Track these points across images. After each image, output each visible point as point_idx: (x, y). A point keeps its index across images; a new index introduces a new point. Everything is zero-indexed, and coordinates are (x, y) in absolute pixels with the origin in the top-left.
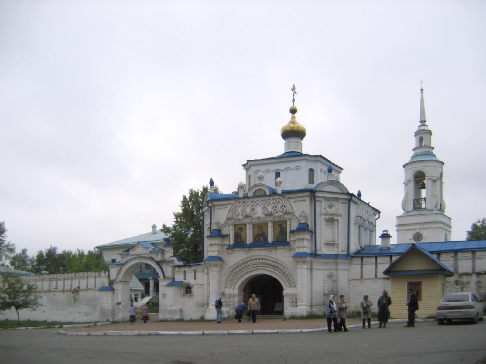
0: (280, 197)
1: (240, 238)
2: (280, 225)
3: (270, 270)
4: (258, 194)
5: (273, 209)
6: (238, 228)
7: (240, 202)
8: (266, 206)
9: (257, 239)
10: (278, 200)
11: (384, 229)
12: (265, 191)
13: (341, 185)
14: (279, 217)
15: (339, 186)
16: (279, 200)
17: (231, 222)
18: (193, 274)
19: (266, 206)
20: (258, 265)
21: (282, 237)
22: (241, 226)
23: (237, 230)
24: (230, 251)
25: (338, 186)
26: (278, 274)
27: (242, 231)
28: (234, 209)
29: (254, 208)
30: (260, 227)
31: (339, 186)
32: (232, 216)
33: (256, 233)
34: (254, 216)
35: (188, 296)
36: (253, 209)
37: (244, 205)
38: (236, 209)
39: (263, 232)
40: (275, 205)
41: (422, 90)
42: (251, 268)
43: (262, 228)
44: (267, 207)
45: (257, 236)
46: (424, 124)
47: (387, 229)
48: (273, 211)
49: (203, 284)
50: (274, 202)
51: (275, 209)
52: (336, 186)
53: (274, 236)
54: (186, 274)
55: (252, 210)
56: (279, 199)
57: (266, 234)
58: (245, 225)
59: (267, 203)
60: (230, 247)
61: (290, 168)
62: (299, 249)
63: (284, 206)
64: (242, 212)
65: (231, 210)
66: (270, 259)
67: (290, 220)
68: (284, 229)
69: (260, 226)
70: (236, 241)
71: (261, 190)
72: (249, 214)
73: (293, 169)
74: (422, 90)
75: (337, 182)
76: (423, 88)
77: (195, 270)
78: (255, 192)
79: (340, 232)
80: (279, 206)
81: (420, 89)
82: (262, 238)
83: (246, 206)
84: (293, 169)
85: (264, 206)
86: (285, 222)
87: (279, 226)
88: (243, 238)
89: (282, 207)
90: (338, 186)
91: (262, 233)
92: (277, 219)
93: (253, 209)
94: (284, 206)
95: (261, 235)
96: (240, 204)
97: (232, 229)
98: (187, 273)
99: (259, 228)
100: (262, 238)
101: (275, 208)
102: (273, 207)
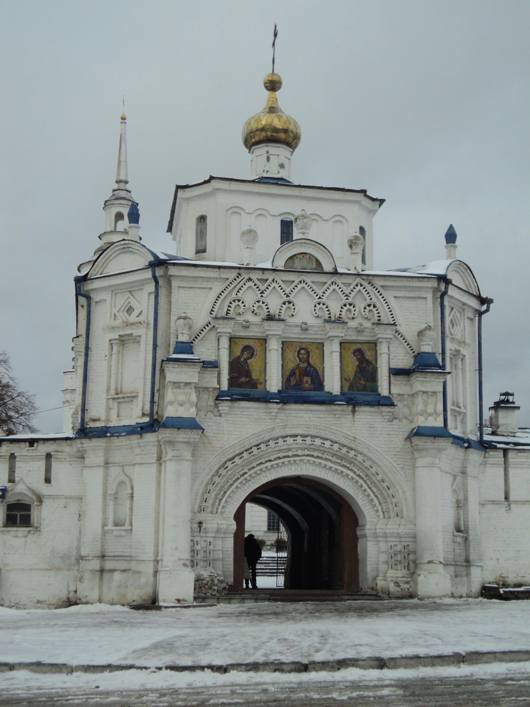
0: (363, 282)
1: (248, 373)
2: (359, 353)
3: (330, 468)
4: (298, 265)
5: (345, 308)
6: (240, 347)
7: (250, 279)
8: (324, 300)
9: (293, 382)
10: (332, 288)
11: (504, 391)
12: (317, 261)
13: (470, 276)
14: (360, 331)
15: (467, 278)
16: (359, 287)
17: (227, 328)
18: (42, 464)
19: (324, 300)
20: (300, 452)
21: (363, 382)
22: (251, 343)
23: (237, 352)
24: (224, 406)
25: (464, 277)
26: (353, 478)
27: (252, 356)
28: (233, 296)
29: (291, 298)
30: (303, 352)
31: (467, 278)
32: (227, 313)
33: (291, 366)
34: (291, 321)
35: (26, 534)
36: (290, 302)
37: (262, 288)
38: (239, 295)
39: (309, 364)
40: (350, 300)
41: (123, 119)
42: (279, 458)
43: (308, 353)
44: (327, 303)
45: (293, 373)
46: (125, 186)
47: (510, 391)
48: (343, 313)
49: (482, 505)
50: (347, 292)
51: (349, 310)
52: (461, 276)
53: (343, 378)
54: (18, 464)
55: (284, 303)
56: (361, 285)
57: (320, 373)
58: (264, 341)
59: (329, 291)
60: (220, 396)
61: (321, 217)
62: (426, 419)
63: (374, 306)
64: (256, 306)
65: (222, 298)
66: (333, 438)
67: (389, 341)
68: (368, 362)
69: (303, 349)
70: (232, 382)
71: (308, 256)
72: (277, 312)
73: (326, 220)
74: (123, 119)
75: (466, 267)
76: (127, 115)
77: (49, 456)
78: (291, 258)
79: (468, 385)
80: (360, 304)
81: (121, 115)
82: (307, 379)
83: (268, 291)
84: (326, 220)
85: (288, 296)
86: (374, 345)
87: (354, 353)
88: (255, 375)
89: (368, 308)
90: (464, 277)
91: (307, 367)
92: (354, 337)
93: (290, 302)
94: (374, 306)
95: (305, 372)
96: (250, 284)
97: (277, 350)
98: (19, 461)
99: (299, 353)
100: (307, 379)
101: (348, 306)
102: (345, 305)
